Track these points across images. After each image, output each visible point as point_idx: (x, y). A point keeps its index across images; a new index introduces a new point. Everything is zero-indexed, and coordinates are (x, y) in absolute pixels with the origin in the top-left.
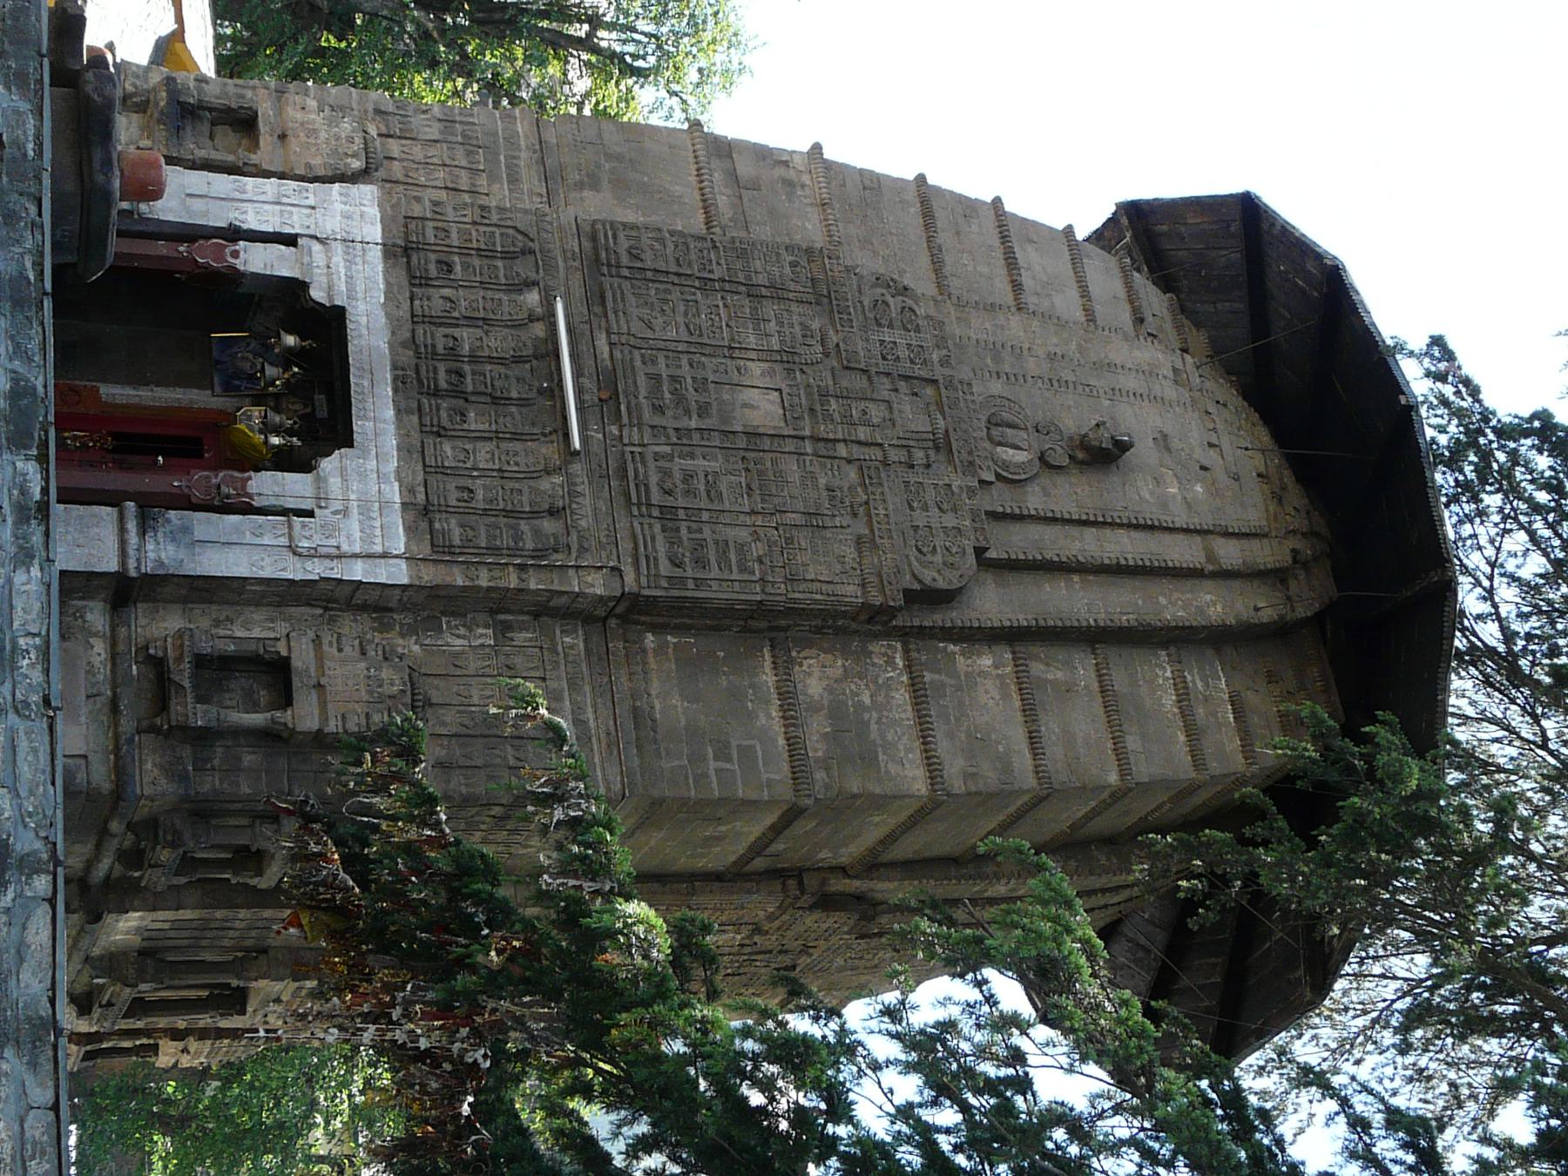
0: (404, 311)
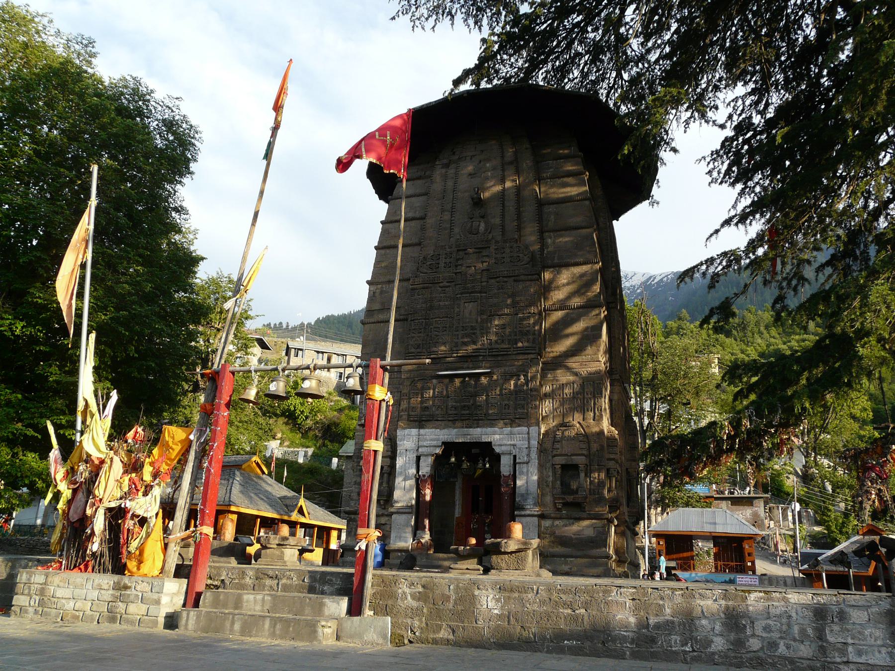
0: (443, 423)
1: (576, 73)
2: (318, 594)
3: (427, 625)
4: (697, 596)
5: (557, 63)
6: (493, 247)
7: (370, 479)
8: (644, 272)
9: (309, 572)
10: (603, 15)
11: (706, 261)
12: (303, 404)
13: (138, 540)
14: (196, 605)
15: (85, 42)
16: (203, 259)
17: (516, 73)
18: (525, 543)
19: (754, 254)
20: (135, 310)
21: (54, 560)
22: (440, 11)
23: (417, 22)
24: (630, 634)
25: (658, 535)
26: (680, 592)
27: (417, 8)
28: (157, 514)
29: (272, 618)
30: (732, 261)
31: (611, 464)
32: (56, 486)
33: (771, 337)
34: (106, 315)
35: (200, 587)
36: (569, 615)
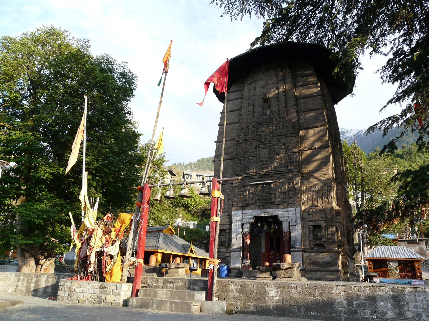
1: (312, 34)
2: (192, 290)
3: (244, 304)
4: (378, 290)
5: (302, 30)
6: (274, 122)
7: (214, 235)
8: (356, 129)
9: (188, 280)
10: (323, 4)
11: (381, 122)
12: (191, 201)
13: (110, 266)
14: (137, 295)
15: (85, 41)
16: (141, 135)
17: (282, 37)
18: (292, 265)
19: (406, 117)
20: (111, 160)
21: (74, 275)
22: (244, 11)
23: (233, 17)
24: (344, 309)
25: (368, 260)
26: (369, 288)
27: (232, 10)
28: (118, 254)
29: (170, 302)
30: (394, 121)
31: (338, 225)
32: (74, 242)
33: (425, 158)
34: (98, 163)
35: (138, 287)
36: (312, 299)
